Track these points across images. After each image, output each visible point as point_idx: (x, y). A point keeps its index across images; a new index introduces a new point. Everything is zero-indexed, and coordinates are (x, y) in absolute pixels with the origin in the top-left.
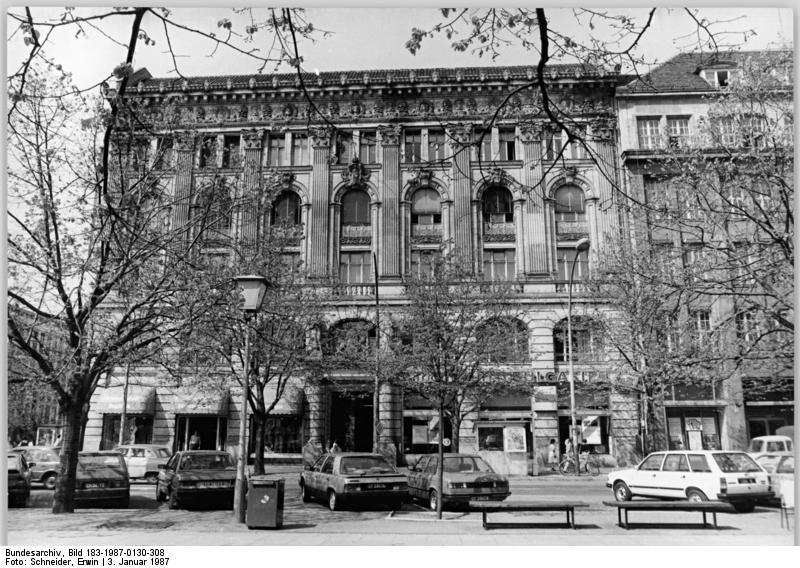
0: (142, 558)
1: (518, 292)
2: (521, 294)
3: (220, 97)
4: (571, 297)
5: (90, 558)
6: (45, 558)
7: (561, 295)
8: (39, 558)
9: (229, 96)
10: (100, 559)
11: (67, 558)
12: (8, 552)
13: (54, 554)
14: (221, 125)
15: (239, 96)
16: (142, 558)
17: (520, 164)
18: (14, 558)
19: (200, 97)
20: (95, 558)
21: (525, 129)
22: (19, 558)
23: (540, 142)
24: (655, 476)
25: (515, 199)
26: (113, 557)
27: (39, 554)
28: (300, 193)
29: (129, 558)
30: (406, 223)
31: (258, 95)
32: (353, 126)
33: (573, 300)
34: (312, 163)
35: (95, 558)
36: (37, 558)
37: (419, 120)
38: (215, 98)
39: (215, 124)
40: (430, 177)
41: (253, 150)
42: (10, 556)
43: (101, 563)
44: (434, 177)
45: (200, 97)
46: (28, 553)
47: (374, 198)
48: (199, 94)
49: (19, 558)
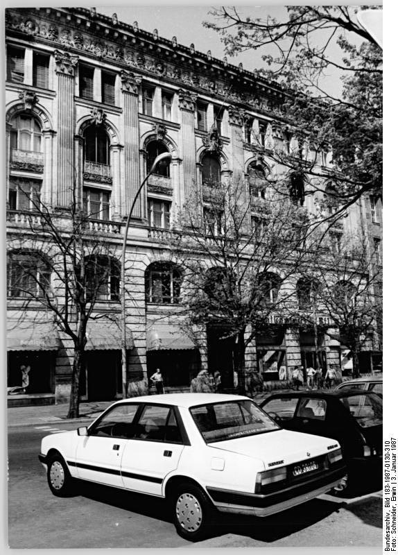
0: (391, 456)
1: (115, 232)
2: (116, 235)
3: (103, 29)
4: (127, 239)
5: (391, 493)
6: (391, 524)
7: (116, 235)
8: (391, 528)
9: (112, 32)
10: (392, 486)
11: (391, 509)
12: (387, 550)
13: (389, 518)
14: (100, 59)
15: (121, 35)
16: (391, 456)
17: (118, 111)
18: (391, 545)
19: (84, 22)
20: (391, 489)
21: (61, 60)
22: (391, 541)
23: (73, 77)
24: (117, 447)
25: (112, 143)
26: (390, 477)
27: (388, 528)
28: (111, 132)
29: (391, 466)
30: (79, 160)
31: (138, 42)
32: (157, 82)
33: (128, 242)
34: (179, 122)
35: (391, 489)
36: (391, 529)
37: (254, 111)
38: (116, 35)
39: (92, 52)
40: (33, 102)
41: (65, 75)
42: (390, 548)
43: (394, 485)
44: (37, 102)
45: (84, 22)
46: (388, 536)
47: (114, 141)
48: (84, 18)
49: (391, 541)
